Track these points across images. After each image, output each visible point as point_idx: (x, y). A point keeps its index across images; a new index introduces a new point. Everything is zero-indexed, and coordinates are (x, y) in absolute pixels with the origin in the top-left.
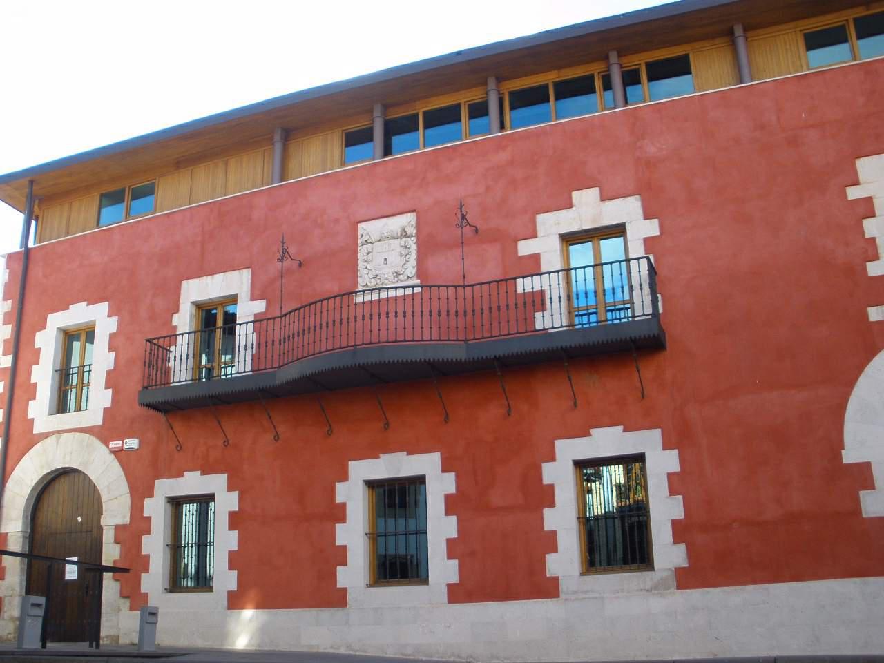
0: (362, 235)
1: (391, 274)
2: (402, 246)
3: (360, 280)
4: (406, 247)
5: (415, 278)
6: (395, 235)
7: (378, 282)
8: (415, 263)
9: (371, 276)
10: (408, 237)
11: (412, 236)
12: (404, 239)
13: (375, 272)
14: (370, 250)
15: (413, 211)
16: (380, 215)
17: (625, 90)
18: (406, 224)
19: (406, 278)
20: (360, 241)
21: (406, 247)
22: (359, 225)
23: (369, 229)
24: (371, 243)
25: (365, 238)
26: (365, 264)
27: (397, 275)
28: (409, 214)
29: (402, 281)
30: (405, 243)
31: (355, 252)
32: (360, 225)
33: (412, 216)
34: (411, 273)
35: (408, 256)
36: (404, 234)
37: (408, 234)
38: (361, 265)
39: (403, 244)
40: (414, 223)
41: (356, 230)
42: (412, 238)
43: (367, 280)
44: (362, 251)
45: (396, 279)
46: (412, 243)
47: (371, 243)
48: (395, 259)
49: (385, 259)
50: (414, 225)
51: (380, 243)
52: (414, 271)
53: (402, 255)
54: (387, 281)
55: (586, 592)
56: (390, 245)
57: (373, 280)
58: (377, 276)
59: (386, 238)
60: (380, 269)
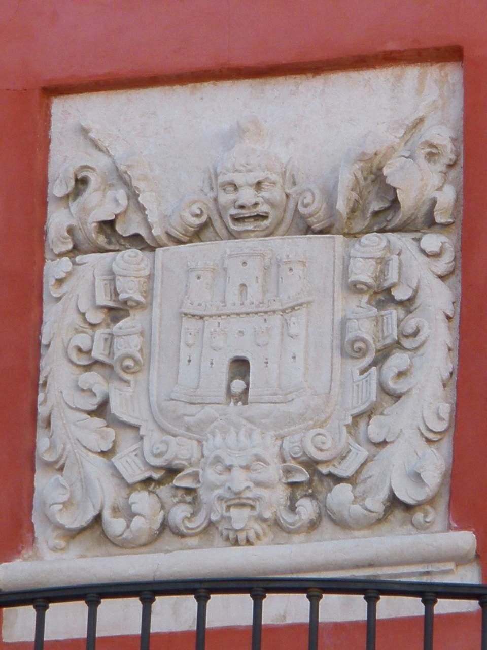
0: (81, 183)
1: (273, 472)
2: (355, 288)
3: (45, 485)
4: (383, 296)
5: (438, 515)
6: (314, 207)
7: (179, 514)
8: (446, 409)
9: (134, 472)
10: (401, 229)
11: (430, 223)
12: (374, 242)
13: (159, 447)
14: (130, 290)
15: (450, 54)
16: (204, 62)
17: (372, 258)
18: (393, 138)
19: (376, 503)
20: (58, 220)
21: (383, 296)
22: (60, 107)
23: (125, 143)
24: (136, 240)
25: (101, 204)
26: (94, 379)
27: (312, 477)
28: (412, 72)
29: (343, 524)
30: (383, 262)
31: (25, 297)
32: (68, 114)
33: (432, 93)
34: (417, 477)
35: (398, 361)
36: (380, 208)
37: (407, 200)
38: (62, 387)
39: (364, 273)
40: (443, 133)
41: (35, 144)
42: (432, 241)
43: (106, 493)
44: (72, 293)
45: (307, 508)
46: (425, 269)
47: (136, 240)
48: (305, 371)
49: (241, 366)
50: (449, 154)
51: (89, 164)
52: (435, 465)
53: (351, 349)
54: (240, 518)
55: (246, 256)
56: (273, 269)
57: (142, 501)
58: (172, 471)
59: (247, 219)
60: (197, 432)
